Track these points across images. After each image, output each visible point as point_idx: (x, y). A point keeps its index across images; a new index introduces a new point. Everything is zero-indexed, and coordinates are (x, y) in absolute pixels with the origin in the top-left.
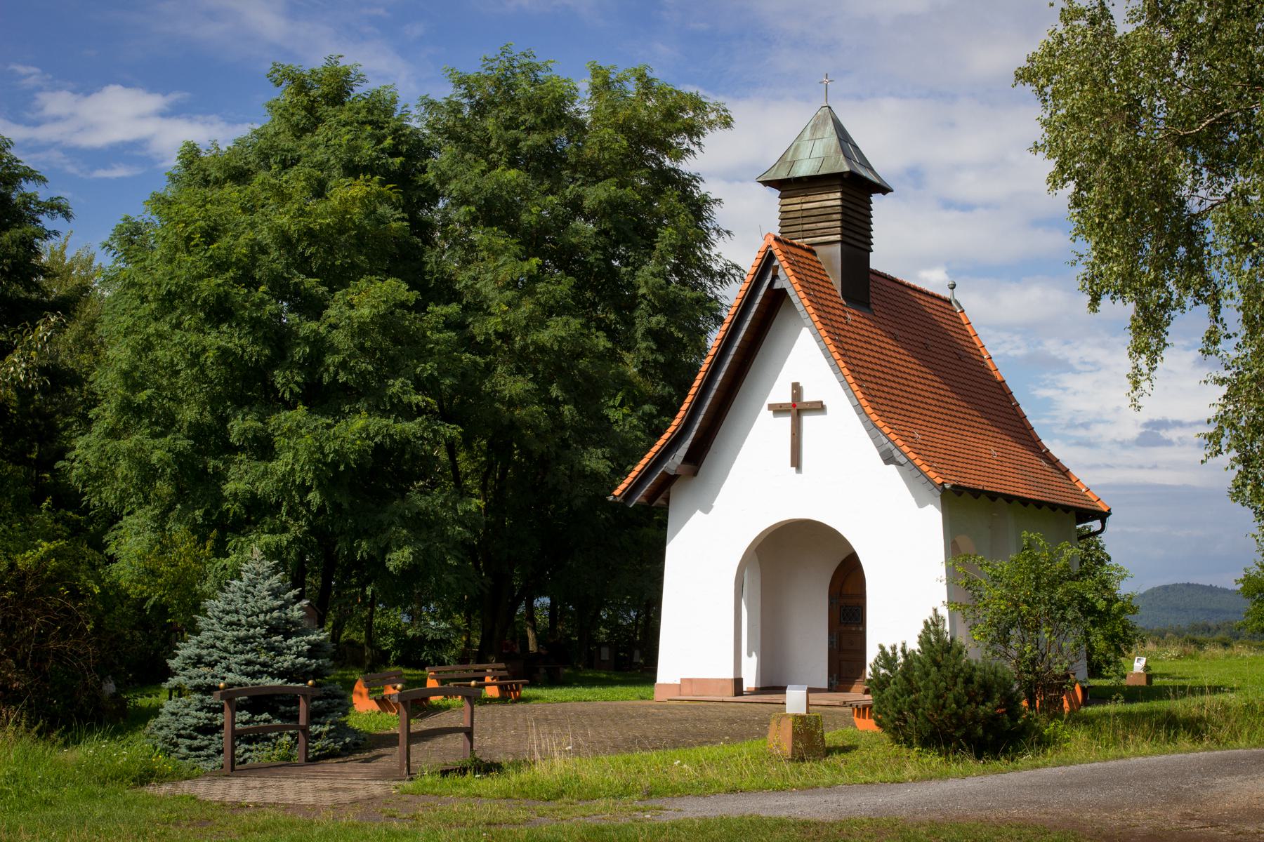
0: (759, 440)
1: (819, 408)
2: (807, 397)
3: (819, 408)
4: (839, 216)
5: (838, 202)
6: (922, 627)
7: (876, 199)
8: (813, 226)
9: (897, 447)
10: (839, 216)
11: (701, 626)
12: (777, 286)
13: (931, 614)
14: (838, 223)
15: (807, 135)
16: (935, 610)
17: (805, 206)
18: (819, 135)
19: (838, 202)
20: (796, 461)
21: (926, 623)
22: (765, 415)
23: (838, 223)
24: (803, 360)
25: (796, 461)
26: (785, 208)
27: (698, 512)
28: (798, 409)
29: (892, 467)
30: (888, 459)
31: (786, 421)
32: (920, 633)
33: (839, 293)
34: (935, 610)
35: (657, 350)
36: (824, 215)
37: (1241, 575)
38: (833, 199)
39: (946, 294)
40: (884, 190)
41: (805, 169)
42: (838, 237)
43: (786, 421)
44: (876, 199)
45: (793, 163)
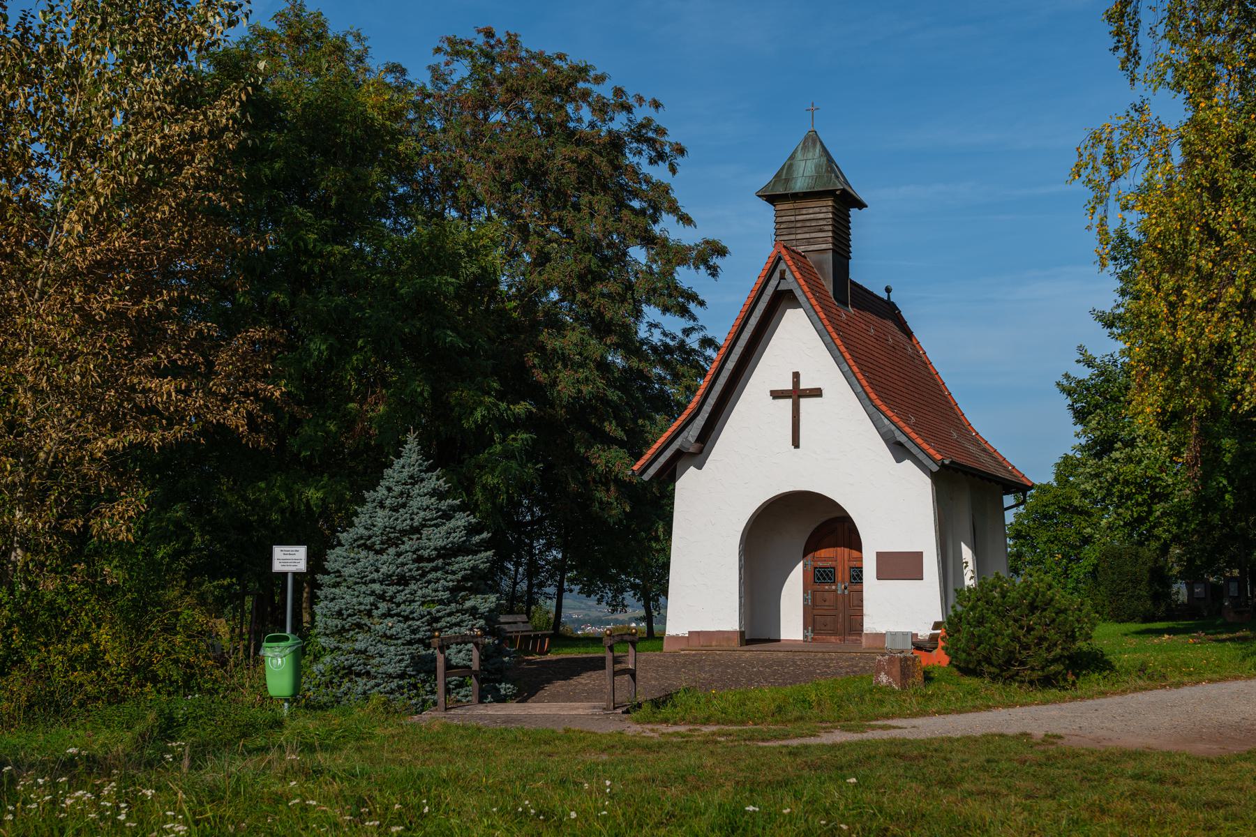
0: (755, 414)
1: (817, 393)
3: (817, 393)
7: (854, 212)
9: (898, 428)
11: (702, 592)
12: (782, 287)
15: (799, 155)
20: (796, 444)
22: (721, 338)
23: (830, 234)
24: (798, 346)
25: (796, 444)
26: (779, 220)
28: (796, 394)
29: (908, 463)
30: (899, 451)
31: (787, 403)
33: (831, 294)
35: (616, 143)
40: (861, 205)
41: (800, 185)
43: (787, 403)
44: (854, 212)
45: (787, 180)
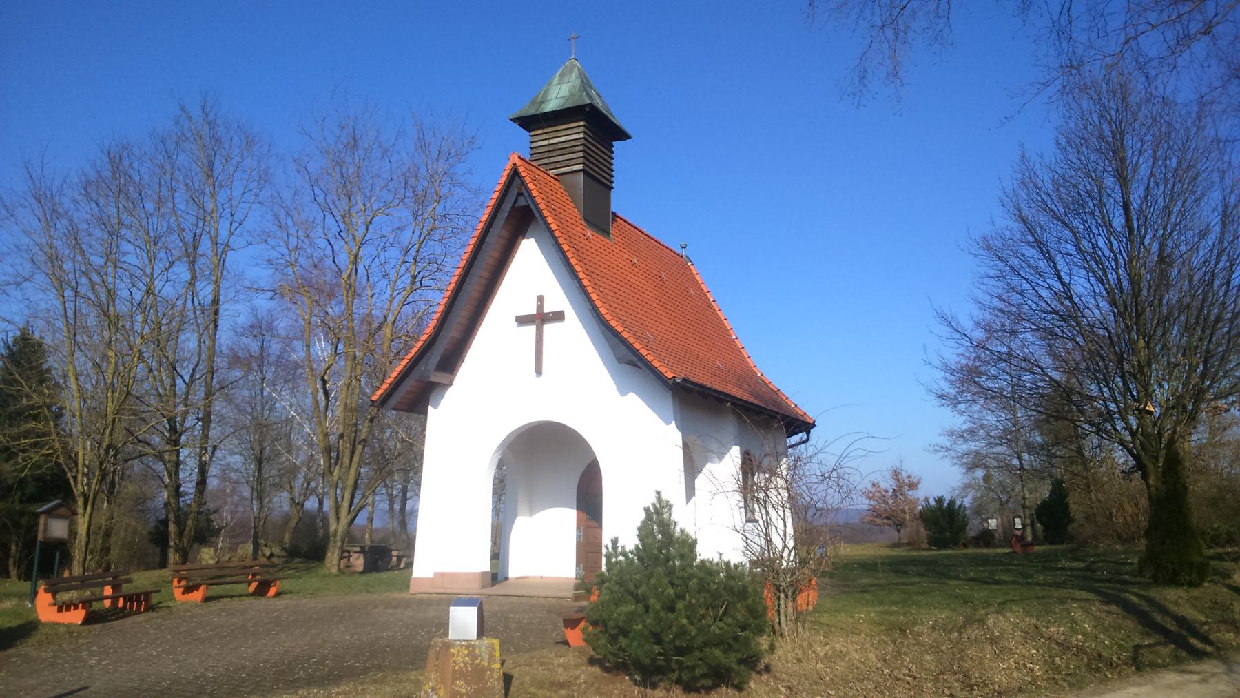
0: (497, 338)
1: (558, 316)
2: (548, 309)
4: (581, 148)
5: (582, 129)
6: (643, 516)
7: (618, 145)
8: (560, 158)
10: (581, 148)
13: (653, 499)
14: (581, 154)
16: (658, 493)
17: (552, 141)
18: (566, 80)
19: (582, 135)
20: (539, 371)
21: (647, 510)
25: (539, 371)
26: (534, 145)
27: (430, 408)
32: (639, 524)
34: (658, 493)
36: (569, 149)
37: (692, 532)
38: (574, 133)
39: (678, 250)
42: (581, 167)
